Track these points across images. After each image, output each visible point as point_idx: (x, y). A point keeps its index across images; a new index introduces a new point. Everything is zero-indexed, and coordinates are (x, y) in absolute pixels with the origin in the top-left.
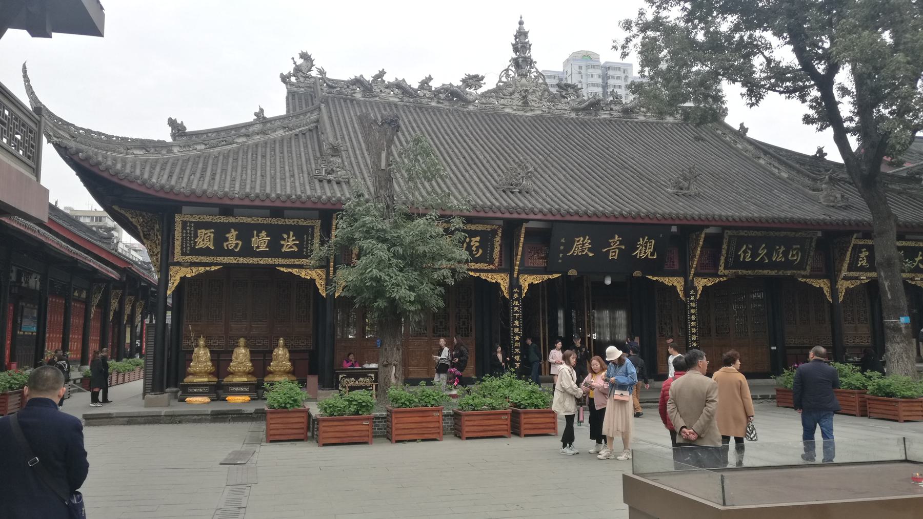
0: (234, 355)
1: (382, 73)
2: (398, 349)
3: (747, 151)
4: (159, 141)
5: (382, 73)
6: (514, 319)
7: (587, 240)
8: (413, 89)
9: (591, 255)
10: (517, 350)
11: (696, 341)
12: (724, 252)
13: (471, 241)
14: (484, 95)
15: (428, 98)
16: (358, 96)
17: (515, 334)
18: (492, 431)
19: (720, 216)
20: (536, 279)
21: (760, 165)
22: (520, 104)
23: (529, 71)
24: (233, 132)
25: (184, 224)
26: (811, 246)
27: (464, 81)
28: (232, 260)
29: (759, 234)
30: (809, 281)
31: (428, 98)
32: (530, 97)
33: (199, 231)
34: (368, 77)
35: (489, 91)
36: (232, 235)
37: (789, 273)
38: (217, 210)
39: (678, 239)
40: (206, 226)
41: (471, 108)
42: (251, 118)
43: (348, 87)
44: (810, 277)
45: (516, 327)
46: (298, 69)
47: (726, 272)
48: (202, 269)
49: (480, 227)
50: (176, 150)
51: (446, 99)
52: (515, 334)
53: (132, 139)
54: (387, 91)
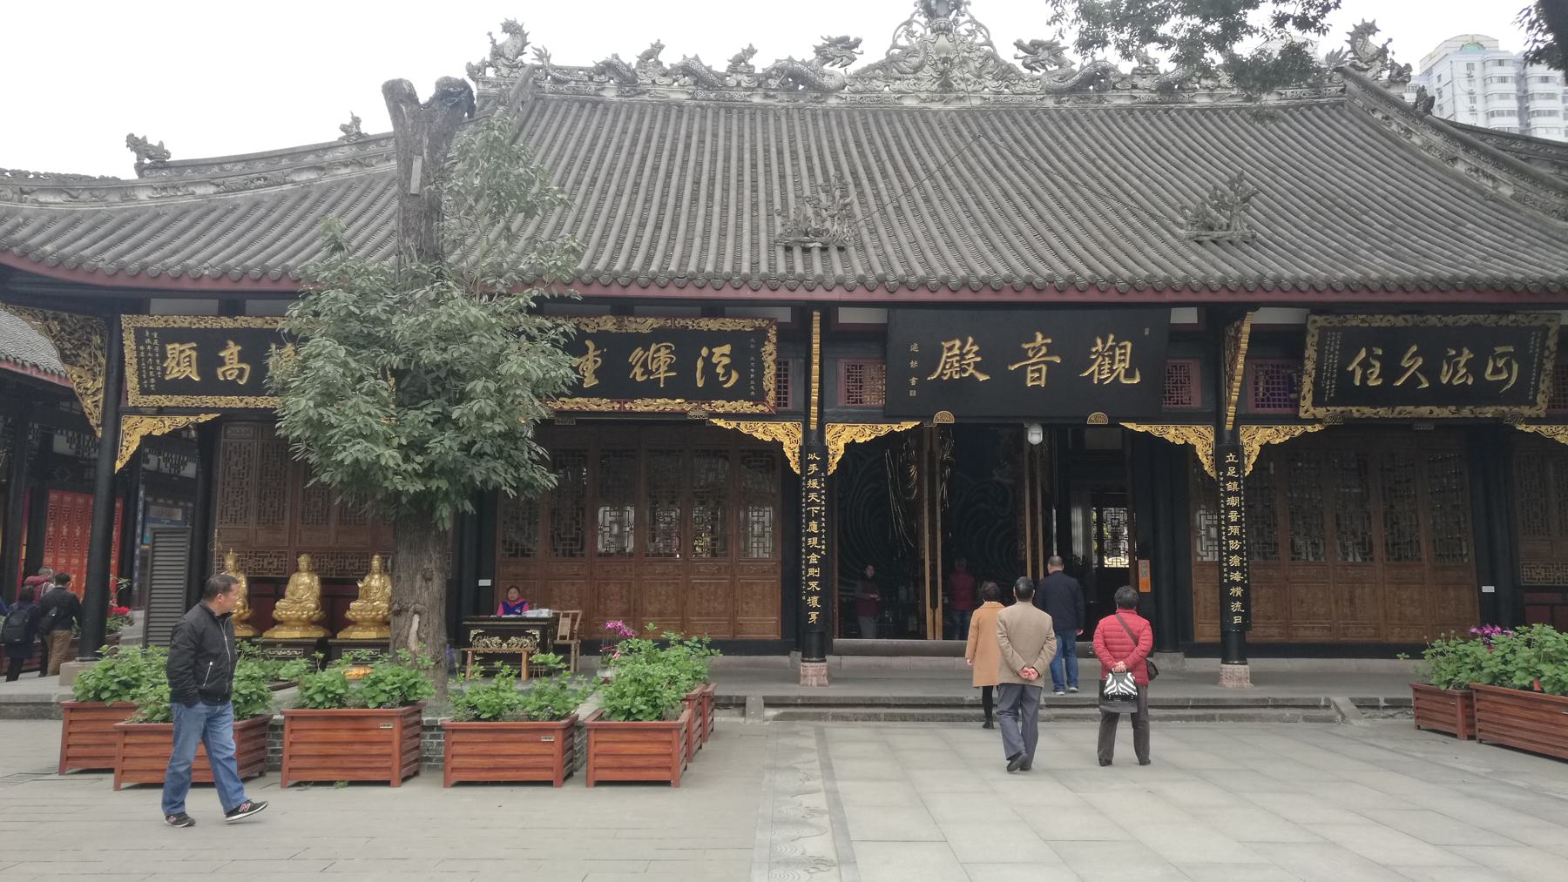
0: (290, 588)
1: (657, 48)
2: (428, 579)
3: (1430, 148)
4: (102, 178)
5: (657, 48)
6: (809, 519)
7: (971, 347)
8: (716, 74)
9: (982, 378)
10: (813, 584)
11: (1240, 569)
12: (1309, 366)
13: (711, 354)
14: (860, 76)
15: (746, 89)
16: (610, 94)
17: (810, 550)
18: (518, 768)
19: (1277, 281)
20: (863, 434)
21: (1457, 177)
22: (935, 87)
23: (955, 21)
24: (285, 162)
25: (140, 334)
26: (1543, 348)
27: (819, 51)
28: (235, 402)
29: (1399, 321)
30: (1545, 430)
31: (746, 89)
32: (956, 73)
33: (169, 347)
34: (630, 58)
35: (872, 68)
36: (231, 352)
37: (1489, 412)
38: (214, 304)
39: (1192, 337)
40: (181, 336)
41: (832, 101)
42: (335, 135)
43: (591, 79)
44: (1549, 420)
45: (812, 535)
46: (497, 53)
47: (1320, 412)
48: (181, 421)
49: (729, 325)
50: (143, 195)
51: (784, 87)
52: (810, 550)
53: (37, 175)
54: (667, 80)
